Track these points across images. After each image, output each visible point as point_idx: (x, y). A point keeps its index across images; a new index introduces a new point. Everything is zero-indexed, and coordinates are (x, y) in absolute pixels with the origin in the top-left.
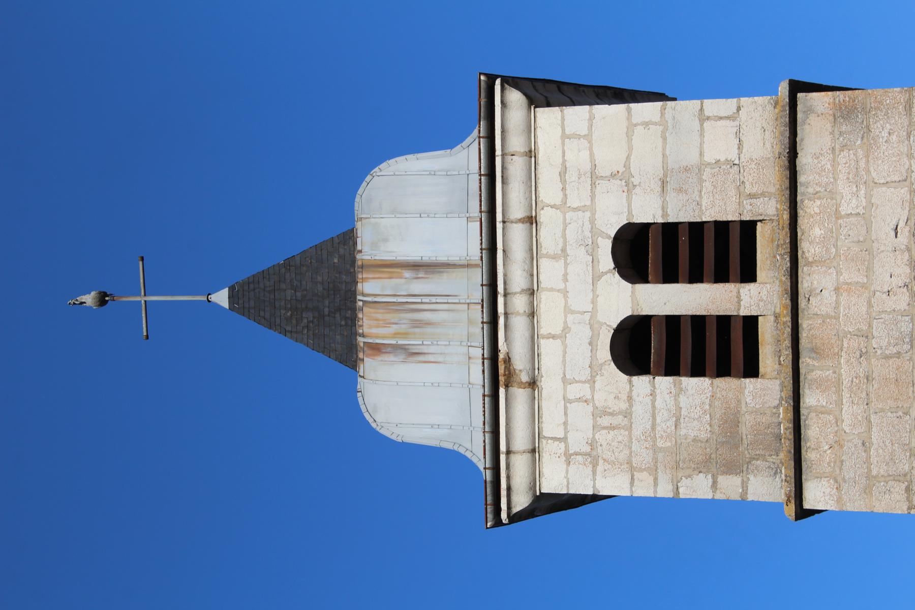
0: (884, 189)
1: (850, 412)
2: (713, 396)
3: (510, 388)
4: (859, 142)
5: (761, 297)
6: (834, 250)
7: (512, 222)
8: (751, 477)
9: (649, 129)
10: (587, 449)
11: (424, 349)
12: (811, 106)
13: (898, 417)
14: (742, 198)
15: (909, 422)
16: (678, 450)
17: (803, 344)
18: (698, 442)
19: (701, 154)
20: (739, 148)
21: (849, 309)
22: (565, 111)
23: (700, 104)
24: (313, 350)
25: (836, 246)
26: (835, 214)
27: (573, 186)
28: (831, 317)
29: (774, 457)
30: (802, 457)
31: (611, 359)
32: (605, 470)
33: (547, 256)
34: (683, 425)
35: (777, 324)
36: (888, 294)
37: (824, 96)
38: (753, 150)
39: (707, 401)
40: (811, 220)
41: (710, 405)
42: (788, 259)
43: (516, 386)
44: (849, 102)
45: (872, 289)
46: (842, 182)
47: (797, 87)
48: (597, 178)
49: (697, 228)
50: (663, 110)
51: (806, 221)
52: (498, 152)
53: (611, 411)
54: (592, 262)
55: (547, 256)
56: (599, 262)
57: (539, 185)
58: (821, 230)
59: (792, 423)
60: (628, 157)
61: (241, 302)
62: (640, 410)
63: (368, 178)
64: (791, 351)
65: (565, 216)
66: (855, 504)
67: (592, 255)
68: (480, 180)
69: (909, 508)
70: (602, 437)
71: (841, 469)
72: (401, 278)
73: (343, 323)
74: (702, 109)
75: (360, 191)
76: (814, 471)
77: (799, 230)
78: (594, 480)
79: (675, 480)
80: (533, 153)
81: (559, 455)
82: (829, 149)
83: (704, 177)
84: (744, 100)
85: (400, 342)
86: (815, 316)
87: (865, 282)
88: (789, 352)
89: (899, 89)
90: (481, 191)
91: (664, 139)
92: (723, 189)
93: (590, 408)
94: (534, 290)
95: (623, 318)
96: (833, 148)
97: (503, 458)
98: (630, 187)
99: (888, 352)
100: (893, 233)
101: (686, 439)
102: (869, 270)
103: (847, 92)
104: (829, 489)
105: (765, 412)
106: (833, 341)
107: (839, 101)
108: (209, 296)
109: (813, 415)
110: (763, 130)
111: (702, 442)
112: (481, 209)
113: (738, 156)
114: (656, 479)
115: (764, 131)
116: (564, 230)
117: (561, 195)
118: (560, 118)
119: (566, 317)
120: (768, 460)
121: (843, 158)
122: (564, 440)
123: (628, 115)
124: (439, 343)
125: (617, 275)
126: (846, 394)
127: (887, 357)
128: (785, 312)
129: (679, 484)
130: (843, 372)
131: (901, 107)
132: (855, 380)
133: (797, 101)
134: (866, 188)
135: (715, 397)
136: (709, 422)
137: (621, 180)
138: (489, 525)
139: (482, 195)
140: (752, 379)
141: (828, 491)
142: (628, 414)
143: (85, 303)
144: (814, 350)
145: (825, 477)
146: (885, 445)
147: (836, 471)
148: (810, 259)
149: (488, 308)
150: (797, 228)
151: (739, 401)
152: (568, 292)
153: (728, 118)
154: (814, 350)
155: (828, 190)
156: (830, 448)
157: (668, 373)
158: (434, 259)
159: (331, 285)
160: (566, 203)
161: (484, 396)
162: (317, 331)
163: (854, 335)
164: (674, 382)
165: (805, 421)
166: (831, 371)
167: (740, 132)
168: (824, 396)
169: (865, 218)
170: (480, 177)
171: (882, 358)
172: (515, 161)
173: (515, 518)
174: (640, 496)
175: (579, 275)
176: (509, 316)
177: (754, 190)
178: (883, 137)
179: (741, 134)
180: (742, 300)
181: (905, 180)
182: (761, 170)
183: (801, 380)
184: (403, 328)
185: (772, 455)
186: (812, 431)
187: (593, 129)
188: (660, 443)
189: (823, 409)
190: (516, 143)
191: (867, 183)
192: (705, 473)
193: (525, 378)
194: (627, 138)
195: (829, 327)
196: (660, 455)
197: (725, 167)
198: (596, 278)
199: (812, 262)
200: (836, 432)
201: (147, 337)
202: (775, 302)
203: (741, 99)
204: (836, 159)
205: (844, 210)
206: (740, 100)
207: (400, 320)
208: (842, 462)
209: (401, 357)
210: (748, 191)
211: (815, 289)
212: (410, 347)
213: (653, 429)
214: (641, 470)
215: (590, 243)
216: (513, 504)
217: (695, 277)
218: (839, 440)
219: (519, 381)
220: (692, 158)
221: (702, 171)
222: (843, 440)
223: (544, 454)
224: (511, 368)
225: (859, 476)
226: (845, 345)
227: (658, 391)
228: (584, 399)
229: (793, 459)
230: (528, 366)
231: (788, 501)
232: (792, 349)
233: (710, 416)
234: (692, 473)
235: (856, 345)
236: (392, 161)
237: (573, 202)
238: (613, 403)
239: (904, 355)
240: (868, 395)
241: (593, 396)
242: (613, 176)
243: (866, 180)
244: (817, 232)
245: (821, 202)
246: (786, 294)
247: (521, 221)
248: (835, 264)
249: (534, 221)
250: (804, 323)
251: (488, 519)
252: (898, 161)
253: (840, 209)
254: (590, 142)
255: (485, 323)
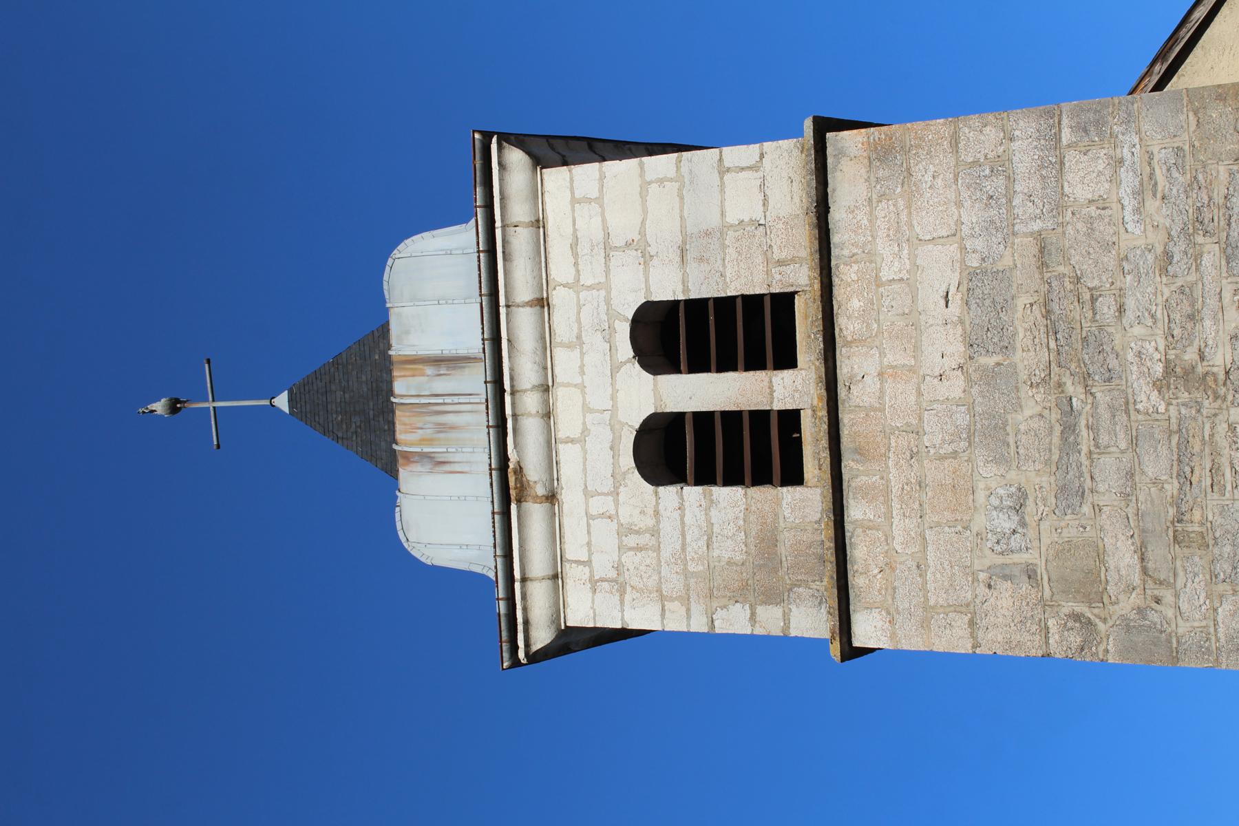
0: (930, 247)
1: (902, 527)
2: (747, 509)
3: (524, 504)
4: (899, 190)
5: (796, 387)
6: (876, 326)
7: (518, 306)
8: (793, 607)
9: (664, 187)
10: (612, 574)
11: (450, 458)
12: (842, 147)
13: (957, 533)
14: (770, 265)
15: (970, 539)
16: (711, 575)
17: (844, 443)
18: (733, 566)
19: (723, 214)
20: (764, 204)
21: (896, 398)
22: (573, 171)
23: (718, 153)
24: (362, 458)
25: (878, 321)
26: (876, 281)
27: (586, 260)
28: (875, 410)
29: (818, 583)
30: (849, 583)
31: (634, 465)
32: (634, 600)
33: (562, 345)
34: (715, 545)
35: (815, 419)
36: (940, 378)
37: (856, 134)
38: (779, 205)
39: (741, 515)
40: (849, 289)
41: (744, 521)
42: (821, 339)
43: (531, 500)
44: (885, 140)
45: (921, 373)
46: (881, 241)
47: (824, 126)
48: (611, 248)
49: (725, 304)
50: (678, 164)
51: (843, 290)
52: (498, 224)
53: (637, 528)
54: (610, 350)
55: (562, 345)
56: (617, 350)
57: (549, 260)
58: (859, 301)
59: (834, 541)
60: (643, 222)
61: (299, 406)
62: (669, 527)
63: (390, 262)
64: (829, 453)
65: (578, 297)
66: (912, 641)
67: (609, 342)
68: (479, 257)
69: (974, 647)
70: (629, 559)
71: (893, 598)
72: (423, 375)
73: (386, 427)
74: (721, 160)
75: (386, 277)
76: (863, 601)
77: (834, 303)
78: (622, 611)
79: (709, 611)
80: (541, 223)
81: (583, 581)
82: (865, 200)
83: (727, 242)
84: (767, 145)
85: (426, 450)
86: (857, 409)
87: (913, 364)
88: (826, 455)
89: (942, 120)
90: (480, 270)
91: (682, 198)
92: (749, 256)
93: (614, 526)
94: (548, 386)
95: (645, 417)
96: (869, 199)
97: (517, 586)
98: (647, 258)
99: (942, 451)
100: (943, 302)
101: (719, 562)
102: (917, 348)
103: (882, 128)
104: (881, 622)
105: (807, 528)
106: (879, 439)
107: (874, 140)
108: (273, 400)
109: (859, 531)
110: (790, 180)
111: (737, 565)
112: (481, 292)
113: (763, 215)
114: (688, 610)
115: (792, 182)
116: (579, 313)
117: (573, 271)
118: (568, 179)
119: (584, 416)
120: (811, 587)
121: (882, 209)
122: (588, 563)
123: (641, 171)
124: (464, 450)
125: (637, 365)
126: (896, 505)
127: (943, 458)
128: (820, 404)
129: (714, 616)
130: (892, 478)
131: (945, 143)
132: (906, 487)
133: (826, 143)
134: (909, 247)
135: (749, 509)
136: (744, 541)
137: (636, 250)
138: (506, 665)
139: (482, 275)
140: (789, 488)
141: (880, 624)
142: (655, 532)
143: (155, 411)
144: (858, 451)
145: (876, 608)
146: (943, 568)
147: (888, 601)
148: (849, 338)
149: (493, 410)
150: (832, 300)
151: (776, 515)
152: (585, 387)
153: (750, 168)
154: (858, 451)
155: (866, 251)
156: (880, 572)
157: (698, 482)
158: (455, 352)
159: (374, 385)
160: (578, 281)
161: (493, 513)
162: (364, 437)
163: (903, 431)
164: (704, 491)
165: (850, 540)
166: (878, 477)
167: (764, 185)
168: (871, 507)
169: (909, 283)
170: (478, 254)
171: (936, 459)
172: (519, 234)
173: (534, 658)
174: (672, 630)
175: (596, 367)
176: (519, 418)
177: (783, 256)
178: (926, 182)
179: (766, 186)
180: (775, 391)
181: (954, 235)
182: (790, 231)
183: (844, 488)
184: (428, 433)
185: (815, 581)
186: (858, 552)
187: (605, 190)
188: (692, 567)
189: (871, 524)
190: (519, 211)
191: (911, 240)
192: (741, 603)
193: (540, 491)
194: (641, 199)
195: (874, 421)
196: (692, 581)
197: (749, 228)
198: (615, 369)
199: (851, 342)
200: (887, 552)
201: (218, 446)
202: (811, 392)
203: (764, 144)
204: (874, 212)
205: (886, 275)
206: (762, 145)
207: (425, 424)
208: (894, 589)
209: (428, 467)
210: (776, 256)
211: (855, 375)
212: (436, 455)
213: (683, 549)
214: (672, 599)
215: (607, 327)
216: (532, 641)
217: (726, 365)
218: (890, 562)
219: (534, 494)
220: (714, 221)
221: (725, 235)
222: (895, 561)
223: (568, 581)
224: (524, 479)
225: (915, 606)
226: (893, 444)
227: (687, 504)
228: (608, 514)
229: (836, 587)
230: (544, 477)
231: (833, 637)
232: (830, 451)
233: (745, 534)
234: (728, 603)
235: (906, 444)
236: (408, 241)
237: (587, 280)
238: (639, 519)
239: (961, 455)
240: (921, 505)
241: (617, 511)
242: (628, 245)
243: (909, 237)
244: (856, 304)
245: (859, 267)
246: (821, 382)
247: (530, 304)
248: (877, 343)
249: (545, 304)
250: (845, 418)
251: (504, 659)
252: (946, 211)
253: (881, 274)
254: (602, 206)
255: (491, 427)
